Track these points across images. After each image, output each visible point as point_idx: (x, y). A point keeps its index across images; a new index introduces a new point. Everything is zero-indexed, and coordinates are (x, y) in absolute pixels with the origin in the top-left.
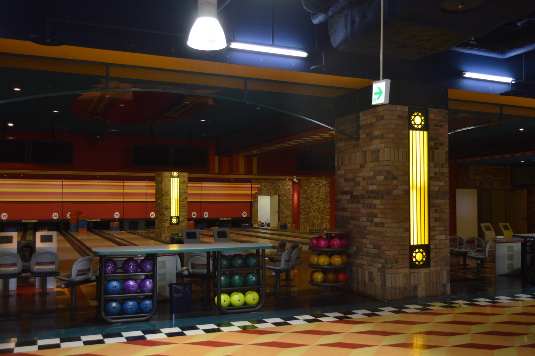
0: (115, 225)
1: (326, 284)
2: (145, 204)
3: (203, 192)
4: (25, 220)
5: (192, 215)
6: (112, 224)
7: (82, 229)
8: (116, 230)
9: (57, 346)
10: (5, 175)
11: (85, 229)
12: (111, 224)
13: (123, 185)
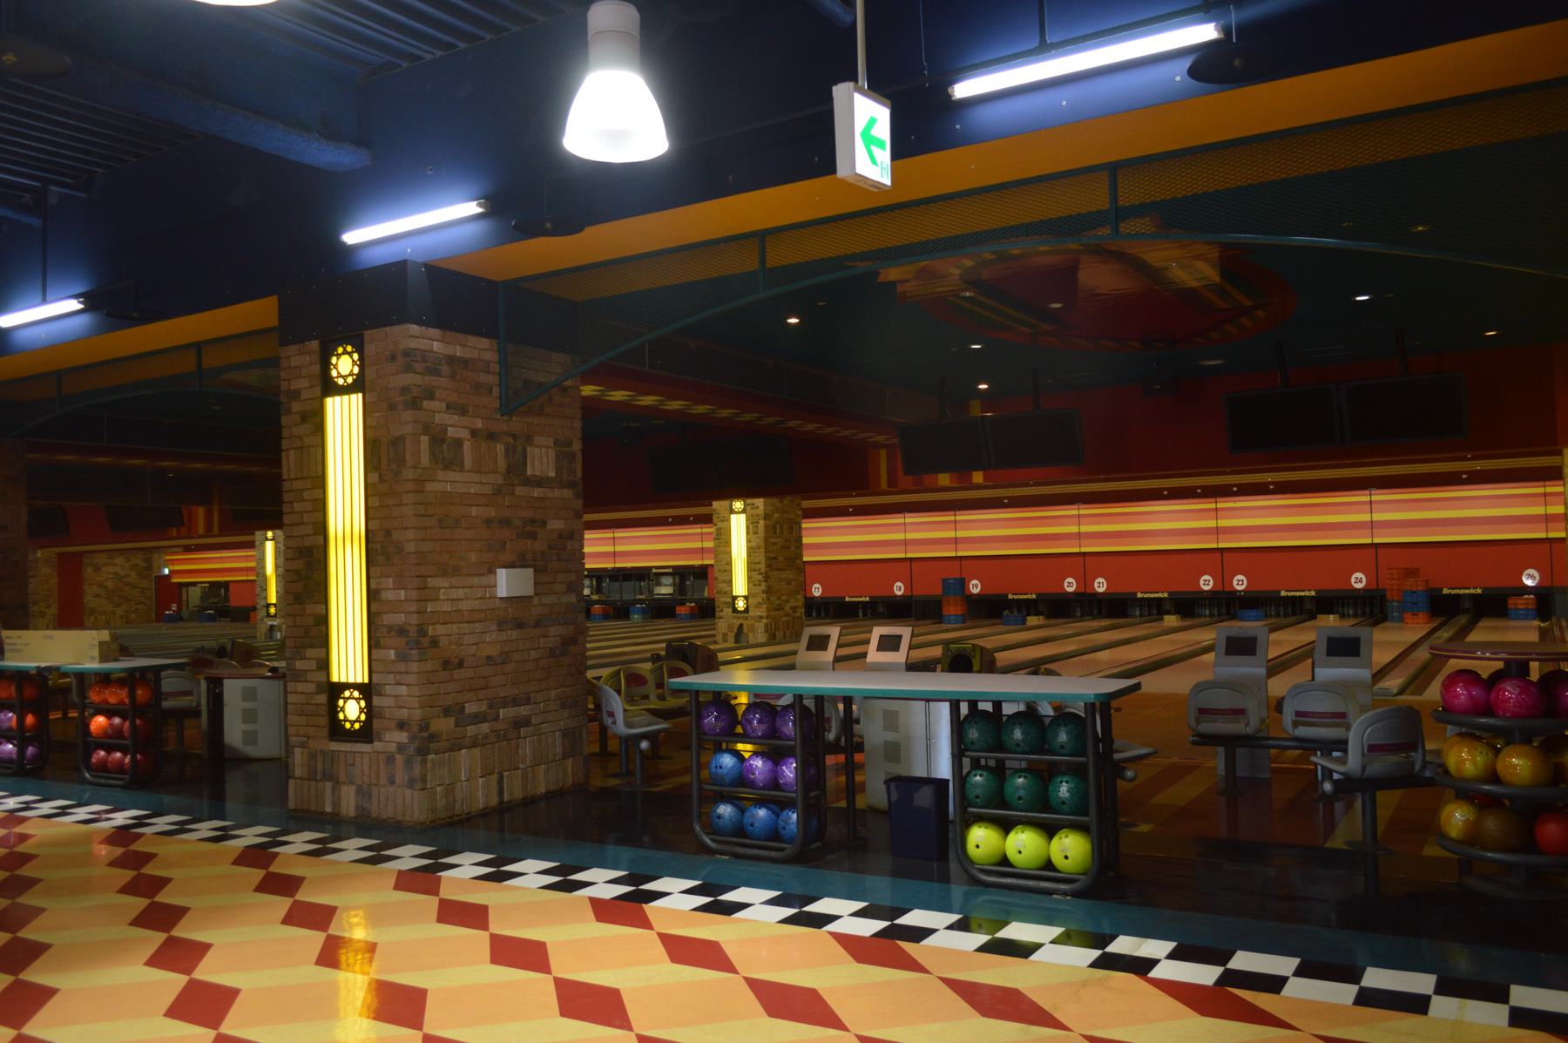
0: (1522, 604)
1: (1490, 855)
2: (1220, 554)
3: (961, 534)
4: (1286, 591)
5: (1066, 584)
6: (1513, 602)
7: (1414, 615)
8: (1526, 618)
9: (1416, 1004)
10: (1235, 489)
11: (1421, 615)
12: (1509, 601)
13: (1216, 509)
